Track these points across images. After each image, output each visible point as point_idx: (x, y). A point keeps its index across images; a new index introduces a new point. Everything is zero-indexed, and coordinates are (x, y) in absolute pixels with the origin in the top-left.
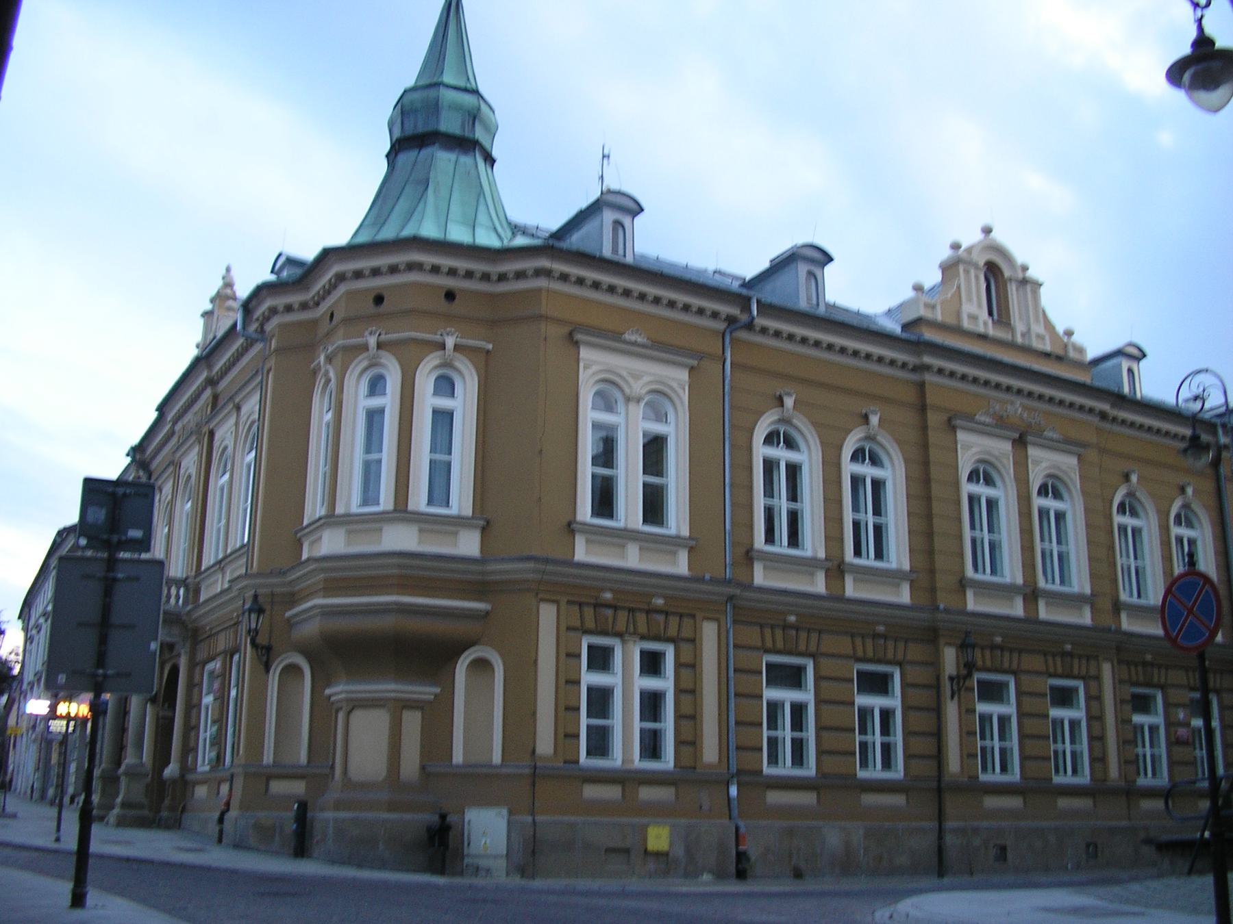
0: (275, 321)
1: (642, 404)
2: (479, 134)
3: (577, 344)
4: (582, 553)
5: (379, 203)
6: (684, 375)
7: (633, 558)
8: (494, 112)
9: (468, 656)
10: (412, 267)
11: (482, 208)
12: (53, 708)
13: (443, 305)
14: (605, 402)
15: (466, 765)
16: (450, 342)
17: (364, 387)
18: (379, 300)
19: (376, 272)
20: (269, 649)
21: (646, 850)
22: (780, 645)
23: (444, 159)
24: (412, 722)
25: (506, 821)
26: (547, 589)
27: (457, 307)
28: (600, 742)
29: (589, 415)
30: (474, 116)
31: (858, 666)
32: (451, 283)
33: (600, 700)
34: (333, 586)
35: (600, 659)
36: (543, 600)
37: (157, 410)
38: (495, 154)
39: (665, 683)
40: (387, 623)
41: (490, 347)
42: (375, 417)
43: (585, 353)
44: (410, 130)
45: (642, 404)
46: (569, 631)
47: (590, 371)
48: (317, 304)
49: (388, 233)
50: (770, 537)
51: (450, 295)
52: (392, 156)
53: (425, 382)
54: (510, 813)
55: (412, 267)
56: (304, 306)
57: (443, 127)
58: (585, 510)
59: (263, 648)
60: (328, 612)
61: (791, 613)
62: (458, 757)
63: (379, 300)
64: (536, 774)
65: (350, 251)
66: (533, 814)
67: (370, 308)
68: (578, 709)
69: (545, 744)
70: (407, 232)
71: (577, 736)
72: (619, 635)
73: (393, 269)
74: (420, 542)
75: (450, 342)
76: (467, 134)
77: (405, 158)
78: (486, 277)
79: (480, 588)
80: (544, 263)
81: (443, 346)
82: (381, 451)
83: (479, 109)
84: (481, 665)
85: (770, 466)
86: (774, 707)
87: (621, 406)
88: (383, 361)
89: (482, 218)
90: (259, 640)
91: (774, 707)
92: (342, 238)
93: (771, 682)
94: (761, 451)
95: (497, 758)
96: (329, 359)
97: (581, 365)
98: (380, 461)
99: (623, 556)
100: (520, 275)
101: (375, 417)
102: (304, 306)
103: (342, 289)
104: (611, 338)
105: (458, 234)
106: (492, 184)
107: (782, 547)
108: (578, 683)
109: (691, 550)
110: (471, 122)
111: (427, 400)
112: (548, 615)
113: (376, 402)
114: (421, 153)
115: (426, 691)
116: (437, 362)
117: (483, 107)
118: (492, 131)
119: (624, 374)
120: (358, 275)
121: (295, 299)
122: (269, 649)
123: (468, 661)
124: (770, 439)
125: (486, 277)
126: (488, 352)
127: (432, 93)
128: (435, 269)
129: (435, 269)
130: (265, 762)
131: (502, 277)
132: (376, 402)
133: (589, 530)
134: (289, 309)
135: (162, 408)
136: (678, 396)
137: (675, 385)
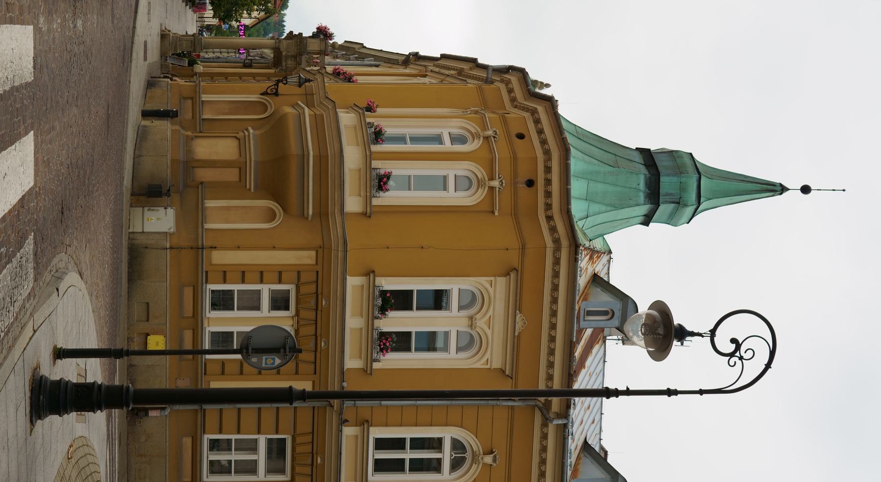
0: (502, 87)
1: (469, 330)
2: (664, 209)
3: (507, 274)
4: (353, 282)
5: (594, 137)
6: (497, 364)
7: (354, 322)
8: (688, 223)
9: (277, 208)
10: (547, 153)
11: (603, 208)
12: (248, 54)
13: (523, 177)
14: (470, 301)
15: (204, 209)
16: (496, 183)
17: (456, 131)
18: (521, 136)
19: (540, 132)
20: (276, 94)
21: (148, 335)
22: (299, 449)
23: (640, 181)
24: (231, 175)
25: (167, 231)
26: (323, 251)
27: (522, 186)
28: (222, 301)
29: (454, 286)
30: (679, 203)
31: (290, 287)
32: (540, 182)
33: (252, 302)
34: (318, 121)
35: (280, 302)
36: (317, 252)
37: (441, 55)
38: (651, 224)
40: (294, 148)
41: (496, 214)
42: (438, 139)
43: (501, 281)
44: (657, 159)
45: (469, 330)
46: (299, 273)
47: (488, 286)
48: (516, 107)
49: (570, 139)
50: (381, 444)
51: (530, 183)
52: (646, 153)
53: (463, 168)
54: (171, 234)
55: (547, 153)
56: (513, 100)
57: (663, 179)
58: (377, 432)
59: (277, 90)
60: (300, 118)
61: (323, 460)
62: (210, 204)
63: (521, 136)
64: (198, 249)
65: (556, 117)
66: (171, 248)
67: (514, 131)
68: (243, 282)
69: (220, 257)
70: (573, 151)
71: (225, 282)
72: (297, 313)
73: (544, 142)
74: (350, 170)
75: (496, 183)
76: (662, 199)
77: (638, 158)
78: (548, 206)
79: (322, 213)
80: (565, 243)
81: (492, 178)
82: (411, 144)
83: (686, 205)
84: (272, 216)
85: (436, 444)
86: (252, 447)
87: (464, 313)
88: (476, 141)
89: (595, 207)
90: (281, 85)
91: (252, 447)
92: (561, 110)
93: (270, 442)
94: (447, 434)
95: (207, 226)
96: (476, 112)
97: (492, 278)
98: (406, 144)
99: (353, 315)
100: (553, 230)
101: (438, 139)
102: (513, 100)
103: (527, 115)
104: (517, 303)
105: (577, 187)
106: (626, 223)
107: (373, 455)
108: (262, 282)
109: (364, 370)
110: (672, 200)
111: (452, 170)
112: (307, 257)
113: (447, 139)
114: (641, 166)
115: (251, 183)
116: (480, 176)
117: (689, 210)
118: (672, 220)
119: (490, 313)
120: (537, 121)
121: (518, 93)
122: (276, 94)
123: (270, 206)
124: (457, 445)
125: (548, 206)
126: (493, 212)
127: (691, 169)
128: (548, 170)
129: (548, 170)
130: (203, 96)
131: (549, 218)
132: (447, 139)
133: (365, 436)
134: (510, 91)
135: (444, 56)
136: (479, 360)
137: (488, 355)
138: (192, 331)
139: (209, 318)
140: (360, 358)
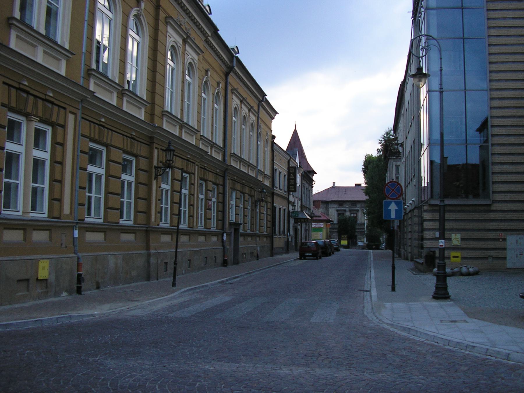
21: (37, 279)
39: (45, 155)
138: (162, 235)
139: (23, 212)
140: (35, 46)
